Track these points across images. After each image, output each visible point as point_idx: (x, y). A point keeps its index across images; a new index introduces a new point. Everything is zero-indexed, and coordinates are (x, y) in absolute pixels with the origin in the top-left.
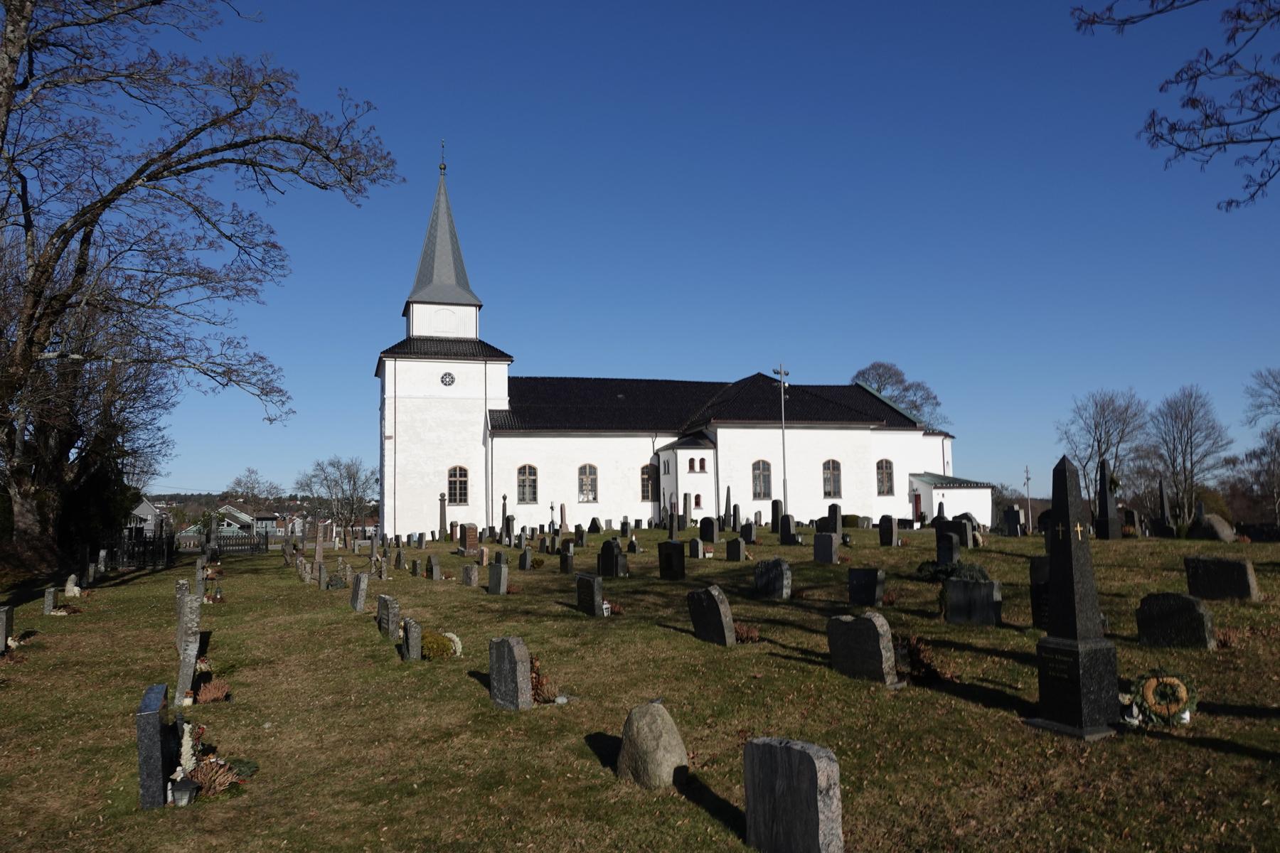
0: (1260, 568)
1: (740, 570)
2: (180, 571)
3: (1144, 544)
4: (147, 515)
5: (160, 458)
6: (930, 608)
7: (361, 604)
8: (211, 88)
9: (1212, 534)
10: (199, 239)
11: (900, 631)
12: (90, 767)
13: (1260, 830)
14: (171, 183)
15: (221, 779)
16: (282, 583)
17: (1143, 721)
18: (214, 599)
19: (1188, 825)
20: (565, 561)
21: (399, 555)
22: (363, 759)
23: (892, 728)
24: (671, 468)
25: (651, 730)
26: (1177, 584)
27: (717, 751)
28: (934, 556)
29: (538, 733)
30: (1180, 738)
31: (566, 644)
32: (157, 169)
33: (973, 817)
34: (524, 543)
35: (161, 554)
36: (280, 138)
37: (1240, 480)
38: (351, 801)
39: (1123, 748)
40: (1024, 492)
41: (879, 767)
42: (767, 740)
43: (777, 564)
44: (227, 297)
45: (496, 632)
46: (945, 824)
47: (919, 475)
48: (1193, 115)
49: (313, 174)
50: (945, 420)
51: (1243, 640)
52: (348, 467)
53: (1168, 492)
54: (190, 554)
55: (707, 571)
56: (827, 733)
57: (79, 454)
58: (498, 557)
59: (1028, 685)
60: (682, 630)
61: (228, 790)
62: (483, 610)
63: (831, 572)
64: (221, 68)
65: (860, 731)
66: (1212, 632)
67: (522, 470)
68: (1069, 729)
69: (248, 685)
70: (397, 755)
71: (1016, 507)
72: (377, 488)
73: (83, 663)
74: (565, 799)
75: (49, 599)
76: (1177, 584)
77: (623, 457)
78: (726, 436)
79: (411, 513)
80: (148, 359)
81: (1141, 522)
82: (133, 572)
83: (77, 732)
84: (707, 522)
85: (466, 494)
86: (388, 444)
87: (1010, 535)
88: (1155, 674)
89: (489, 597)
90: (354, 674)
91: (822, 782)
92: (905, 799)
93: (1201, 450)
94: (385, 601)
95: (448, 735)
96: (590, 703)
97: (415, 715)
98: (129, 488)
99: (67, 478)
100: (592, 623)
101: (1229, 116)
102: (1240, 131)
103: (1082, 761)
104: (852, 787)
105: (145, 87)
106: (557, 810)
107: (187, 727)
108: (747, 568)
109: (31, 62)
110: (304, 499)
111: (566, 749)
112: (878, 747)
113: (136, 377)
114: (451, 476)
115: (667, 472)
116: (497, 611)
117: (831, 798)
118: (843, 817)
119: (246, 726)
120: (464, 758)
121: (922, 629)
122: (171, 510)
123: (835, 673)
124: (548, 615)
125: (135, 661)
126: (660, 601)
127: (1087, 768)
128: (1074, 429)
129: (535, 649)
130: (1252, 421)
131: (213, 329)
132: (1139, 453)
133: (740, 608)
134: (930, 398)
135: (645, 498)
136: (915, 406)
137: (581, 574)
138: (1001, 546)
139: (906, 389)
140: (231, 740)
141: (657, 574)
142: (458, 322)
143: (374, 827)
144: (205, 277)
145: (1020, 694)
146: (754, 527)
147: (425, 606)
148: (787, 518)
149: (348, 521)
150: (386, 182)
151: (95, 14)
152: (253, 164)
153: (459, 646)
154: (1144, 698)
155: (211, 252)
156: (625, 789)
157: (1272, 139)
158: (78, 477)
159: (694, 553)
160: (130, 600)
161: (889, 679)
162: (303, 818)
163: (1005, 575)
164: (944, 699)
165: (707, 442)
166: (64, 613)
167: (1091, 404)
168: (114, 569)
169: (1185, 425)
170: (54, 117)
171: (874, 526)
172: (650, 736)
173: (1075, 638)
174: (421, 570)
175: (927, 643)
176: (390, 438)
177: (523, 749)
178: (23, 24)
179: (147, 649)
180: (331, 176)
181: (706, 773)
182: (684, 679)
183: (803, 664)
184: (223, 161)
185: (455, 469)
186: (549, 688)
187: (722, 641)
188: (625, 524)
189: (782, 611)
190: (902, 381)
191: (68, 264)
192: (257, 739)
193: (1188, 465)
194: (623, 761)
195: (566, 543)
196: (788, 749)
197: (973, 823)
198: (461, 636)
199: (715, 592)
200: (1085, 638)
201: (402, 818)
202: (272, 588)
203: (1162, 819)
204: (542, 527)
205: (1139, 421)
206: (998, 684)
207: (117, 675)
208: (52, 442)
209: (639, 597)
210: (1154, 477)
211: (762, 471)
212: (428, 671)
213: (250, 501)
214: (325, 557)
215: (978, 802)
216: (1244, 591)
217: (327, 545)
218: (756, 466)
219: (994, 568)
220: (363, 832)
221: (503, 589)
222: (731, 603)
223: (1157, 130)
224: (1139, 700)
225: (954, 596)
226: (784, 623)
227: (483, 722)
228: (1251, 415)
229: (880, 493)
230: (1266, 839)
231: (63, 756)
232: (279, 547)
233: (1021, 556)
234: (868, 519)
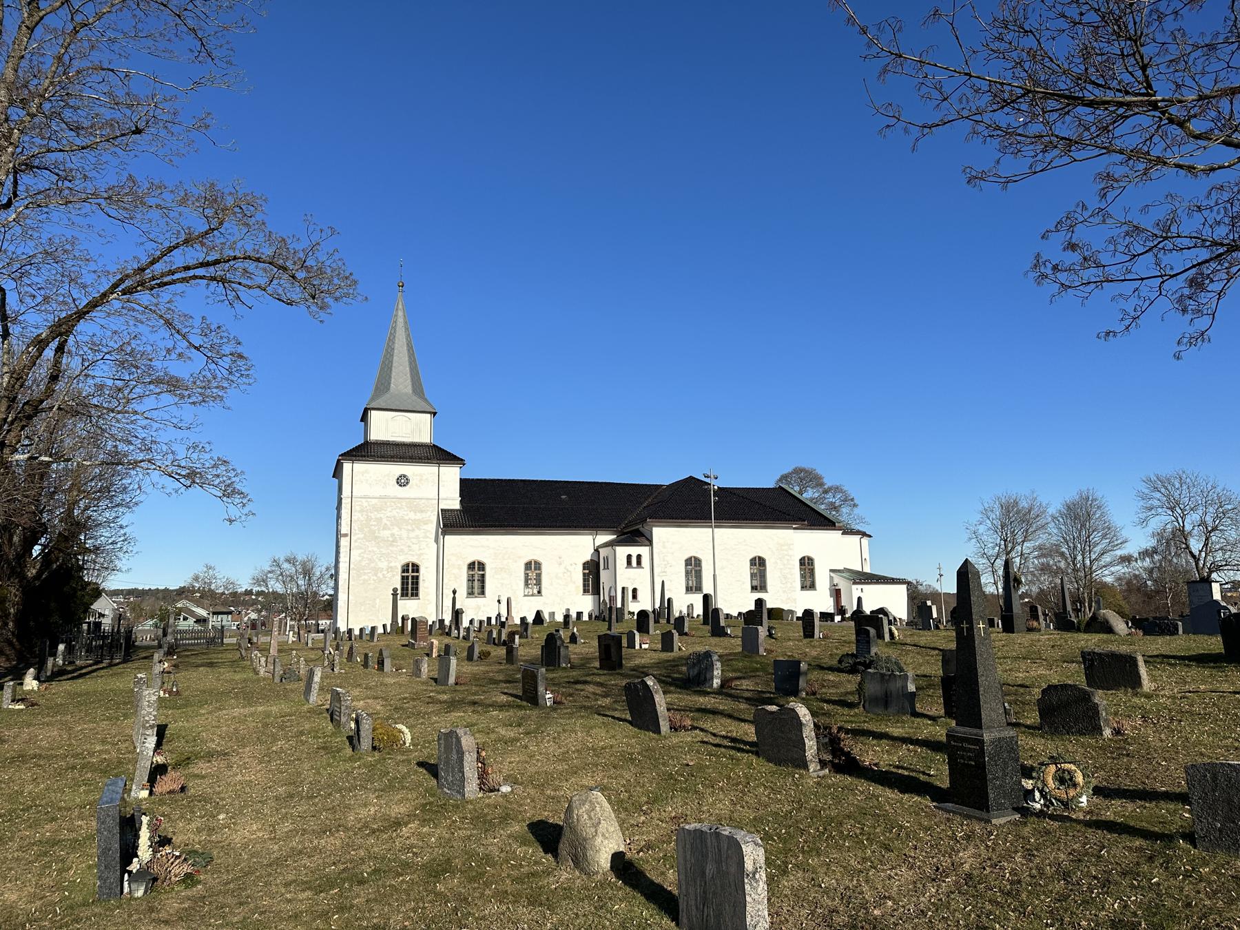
0: (1150, 660)
1: (674, 660)
2: (136, 664)
3: (1047, 636)
4: (104, 608)
5: (121, 555)
6: (850, 699)
7: (314, 697)
8: (186, 210)
9: (1107, 629)
10: (168, 351)
11: (823, 720)
12: (47, 859)
13: (1149, 908)
14: (144, 297)
15: (176, 870)
16: (238, 677)
17: (1045, 805)
18: (170, 693)
19: (1085, 902)
20: (510, 651)
21: (351, 648)
22: (315, 848)
23: (815, 814)
24: (610, 564)
25: (590, 818)
26: (1075, 675)
27: (652, 837)
28: (853, 649)
29: (484, 822)
30: (1078, 821)
31: (510, 733)
32: (134, 283)
33: (889, 898)
34: (472, 635)
35: (120, 647)
36: (249, 258)
37: (1136, 576)
38: (303, 891)
39: (1026, 831)
40: (937, 587)
41: (803, 852)
42: (697, 825)
43: (708, 655)
44: (194, 403)
45: (444, 723)
46: (864, 906)
47: (839, 571)
48: (1074, 258)
49: (280, 291)
50: (862, 520)
51: (1136, 728)
52: (304, 564)
53: (1067, 586)
54: (147, 648)
55: (643, 661)
56: (755, 818)
57: (43, 551)
58: (447, 650)
59: (939, 772)
60: (620, 719)
61: (183, 881)
62: (432, 701)
63: (757, 663)
64: (196, 192)
65: (785, 817)
66: (1106, 720)
67: (471, 566)
68: (977, 813)
69: (203, 777)
70: (348, 844)
71: (929, 603)
72: (332, 584)
73: (40, 755)
74: (509, 886)
75: (7, 693)
76: (1075, 675)
77: (564, 553)
78: (662, 534)
79: (364, 607)
80: (115, 461)
81: (1045, 615)
82: (90, 665)
83: (34, 825)
84: (643, 614)
85: (417, 589)
86: (344, 542)
87: (923, 629)
88: (1054, 760)
89: (439, 688)
90: (306, 766)
91: (749, 866)
92: (827, 882)
93: (1098, 549)
94: (338, 694)
95: (398, 824)
96: (532, 792)
97: (365, 806)
98: (89, 583)
99: (29, 574)
100: (535, 713)
101: (1105, 259)
102: (1115, 272)
103: (989, 844)
104: (777, 870)
105: (125, 209)
106: (501, 896)
107: (145, 819)
108: (681, 658)
109: (15, 183)
110: (259, 593)
111: (509, 836)
112: (802, 832)
113: (100, 477)
114: (403, 571)
115: (606, 568)
116: (445, 702)
117: (757, 881)
118: (769, 900)
119: (201, 817)
120: (412, 846)
121: (843, 718)
122: (128, 604)
123: (762, 761)
124: (494, 705)
125: (91, 754)
126: (599, 690)
127: (994, 850)
128: (982, 529)
129: (481, 738)
130: (1144, 522)
131: (180, 434)
132: (1043, 551)
133: (673, 697)
134: (848, 500)
135: (585, 591)
136: (834, 507)
137: (528, 666)
138: (916, 639)
139: (826, 492)
140: (186, 832)
141: (597, 664)
142: (413, 428)
143: (325, 915)
144: (173, 384)
145: (932, 780)
146: (687, 620)
147: (376, 698)
148: (716, 611)
149: (302, 615)
150: (349, 300)
151: (78, 142)
152: (223, 280)
153: (408, 737)
154: (1045, 784)
155: (181, 362)
156: (565, 876)
157: (1142, 279)
158: (40, 573)
159: (631, 645)
160: (87, 693)
161: (813, 767)
162: (257, 907)
163: (919, 667)
164: (863, 785)
165: (643, 539)
166: (22, 707)
167: (997, 506)
168: (71, 663)
169: (1083, 525)
170: (36, 235)
171: (798, 618)
172: (589, 823)
173: (981, 728)
174: (373, 663)
175: (847, 731)
176: (346, 535)
177: (469, 838)
178: (10, 150)
179: (104, 742)
180: (296, 293)
181: (642, 858)
182: (622, 767)
183: (732, 752)
184: (195, 277)
185: (408, 565)
186: (494, 777)
187: (657, 730)
188: (567, 617)
189: (713, 700)
190: (822, 485)
191: (42, 371)
192: (211, 830)
193: (1088, 562)
194: (564, 848)
195: (511, 635)
196: (717, 835)
197: (890, 903)
198: (410, 727)
199: (650, 682)
200: (988, 728)
201: (352, 906)
202: (227, 681)
203: (1062, 898)
204: (489, 619)
205: (1042, 522)
206: (913, 771)
207: (74, 768)
208: (16, 539)
209: (579, 686)
210: (1056, 573)
211: (693, 566)
212: (378, 762)
213: (207, 596)
214: (279, 651)
215: (895, 883)
216: (1136, 682)
217: (282, 638)
218: (688, 562)
219: (909, 660)
220: (315, 920)
221: (452, 680)
222: (665, 693)
223: (1042, 270)
224: (1040, 785)
225: (872, 688)
226: (714, 712)
227: (430, 812)
228: (1143, 516)
229: (803, 588)
230: (1155, 914)
231: (20, 848)
232: (234, 640)
233: (934, 649)
234: (792, 612)
